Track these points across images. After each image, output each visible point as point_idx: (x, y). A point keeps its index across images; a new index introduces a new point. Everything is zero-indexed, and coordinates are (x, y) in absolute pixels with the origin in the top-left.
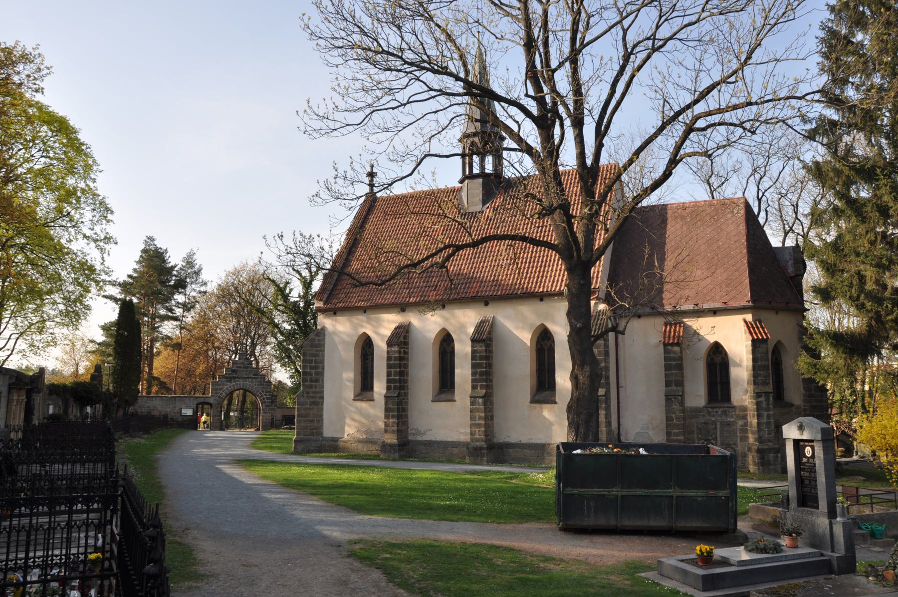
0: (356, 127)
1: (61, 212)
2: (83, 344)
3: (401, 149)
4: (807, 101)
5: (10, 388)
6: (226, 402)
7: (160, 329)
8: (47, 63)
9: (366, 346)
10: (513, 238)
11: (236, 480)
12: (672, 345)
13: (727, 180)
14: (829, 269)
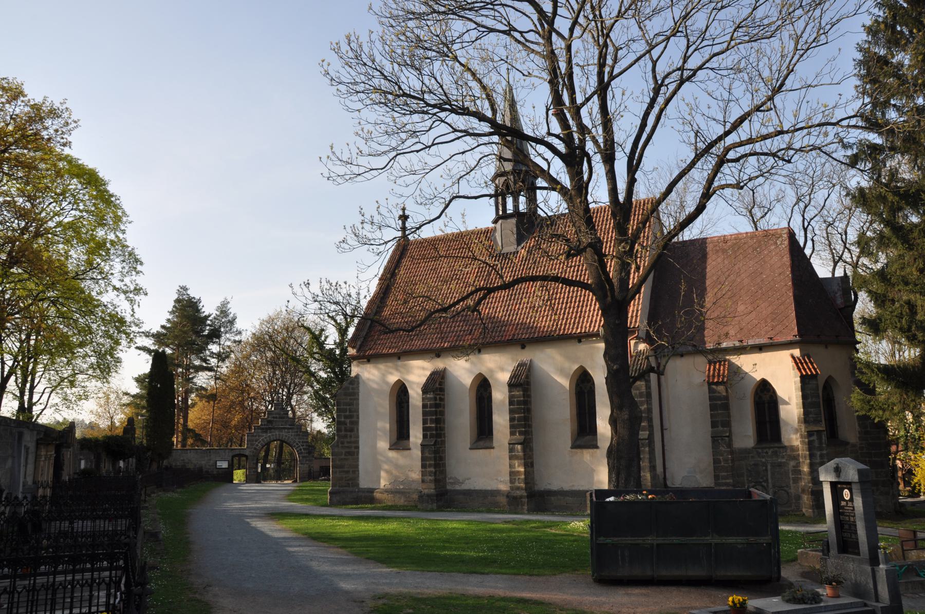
0: (380, 171)
1: (91, 264)
2: (118, 396)
3: (428, 192)
4: (842, 127)
5: (38, 444)
6: (263, 454)
7: (195, 380)
8: (74, 117)
9: (401, 392)
10: (544, 278)
11: (262, 533)
12: (717, 384)
13: (769, 210)
14: (879, 299)
